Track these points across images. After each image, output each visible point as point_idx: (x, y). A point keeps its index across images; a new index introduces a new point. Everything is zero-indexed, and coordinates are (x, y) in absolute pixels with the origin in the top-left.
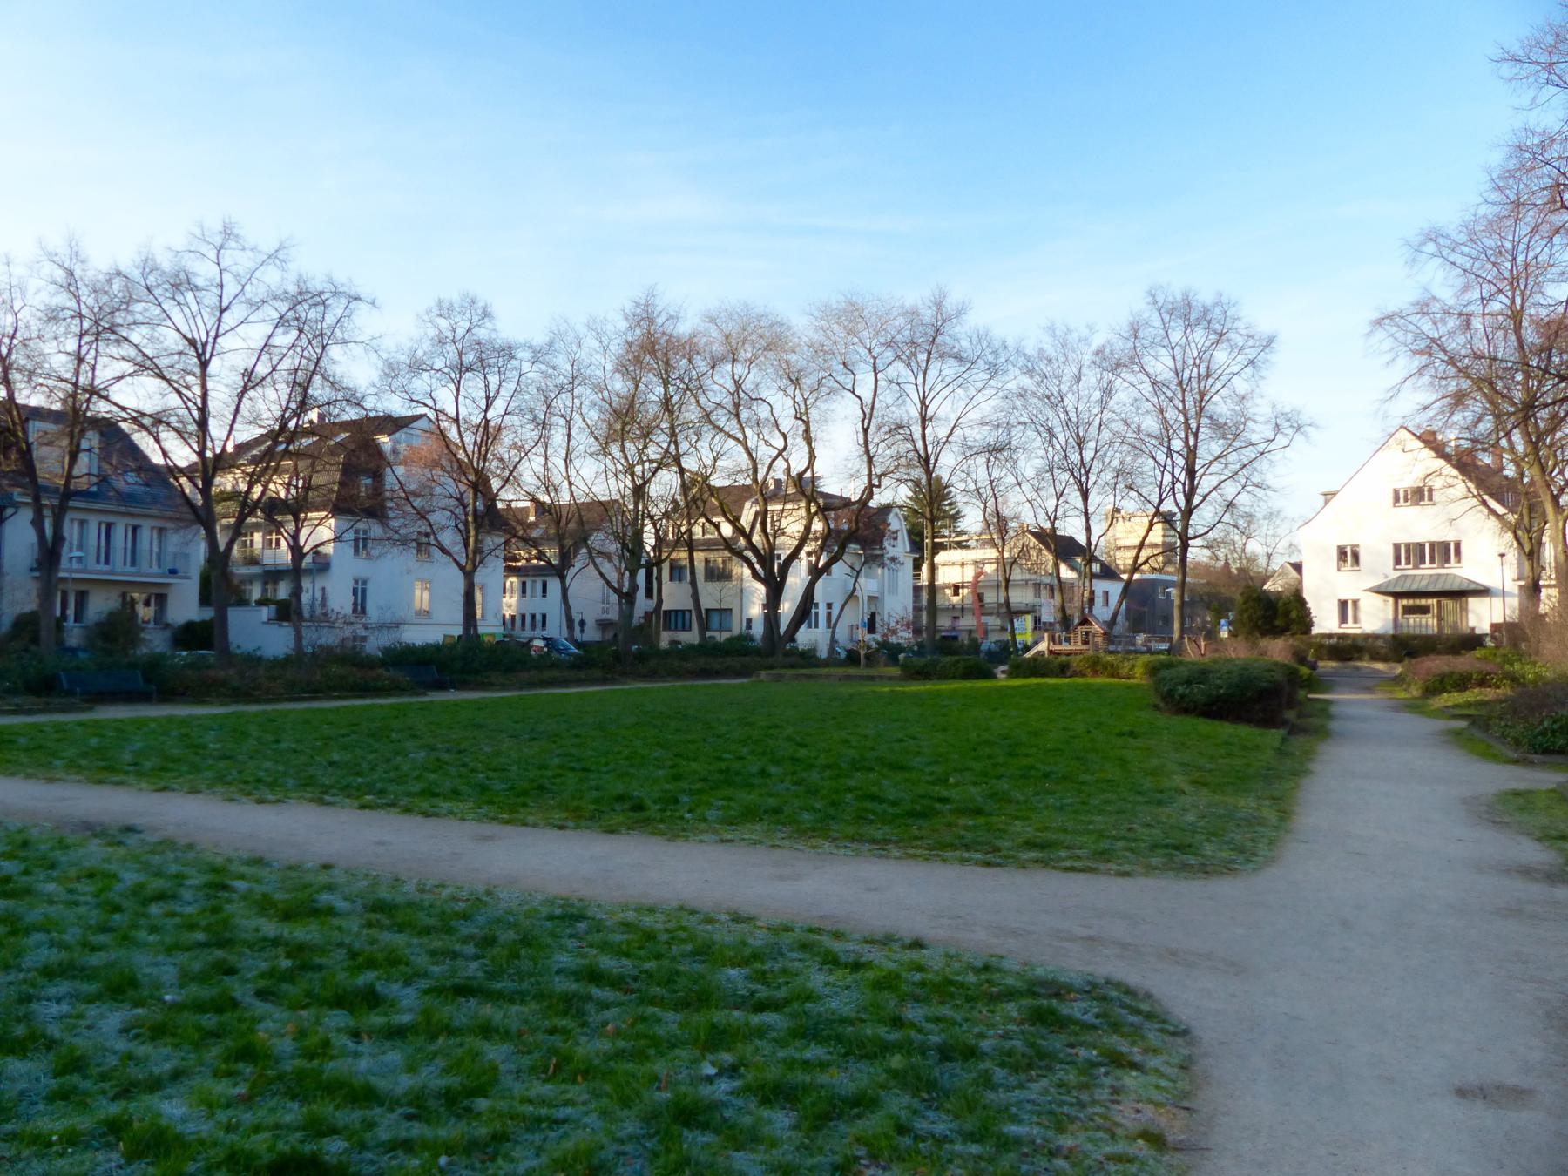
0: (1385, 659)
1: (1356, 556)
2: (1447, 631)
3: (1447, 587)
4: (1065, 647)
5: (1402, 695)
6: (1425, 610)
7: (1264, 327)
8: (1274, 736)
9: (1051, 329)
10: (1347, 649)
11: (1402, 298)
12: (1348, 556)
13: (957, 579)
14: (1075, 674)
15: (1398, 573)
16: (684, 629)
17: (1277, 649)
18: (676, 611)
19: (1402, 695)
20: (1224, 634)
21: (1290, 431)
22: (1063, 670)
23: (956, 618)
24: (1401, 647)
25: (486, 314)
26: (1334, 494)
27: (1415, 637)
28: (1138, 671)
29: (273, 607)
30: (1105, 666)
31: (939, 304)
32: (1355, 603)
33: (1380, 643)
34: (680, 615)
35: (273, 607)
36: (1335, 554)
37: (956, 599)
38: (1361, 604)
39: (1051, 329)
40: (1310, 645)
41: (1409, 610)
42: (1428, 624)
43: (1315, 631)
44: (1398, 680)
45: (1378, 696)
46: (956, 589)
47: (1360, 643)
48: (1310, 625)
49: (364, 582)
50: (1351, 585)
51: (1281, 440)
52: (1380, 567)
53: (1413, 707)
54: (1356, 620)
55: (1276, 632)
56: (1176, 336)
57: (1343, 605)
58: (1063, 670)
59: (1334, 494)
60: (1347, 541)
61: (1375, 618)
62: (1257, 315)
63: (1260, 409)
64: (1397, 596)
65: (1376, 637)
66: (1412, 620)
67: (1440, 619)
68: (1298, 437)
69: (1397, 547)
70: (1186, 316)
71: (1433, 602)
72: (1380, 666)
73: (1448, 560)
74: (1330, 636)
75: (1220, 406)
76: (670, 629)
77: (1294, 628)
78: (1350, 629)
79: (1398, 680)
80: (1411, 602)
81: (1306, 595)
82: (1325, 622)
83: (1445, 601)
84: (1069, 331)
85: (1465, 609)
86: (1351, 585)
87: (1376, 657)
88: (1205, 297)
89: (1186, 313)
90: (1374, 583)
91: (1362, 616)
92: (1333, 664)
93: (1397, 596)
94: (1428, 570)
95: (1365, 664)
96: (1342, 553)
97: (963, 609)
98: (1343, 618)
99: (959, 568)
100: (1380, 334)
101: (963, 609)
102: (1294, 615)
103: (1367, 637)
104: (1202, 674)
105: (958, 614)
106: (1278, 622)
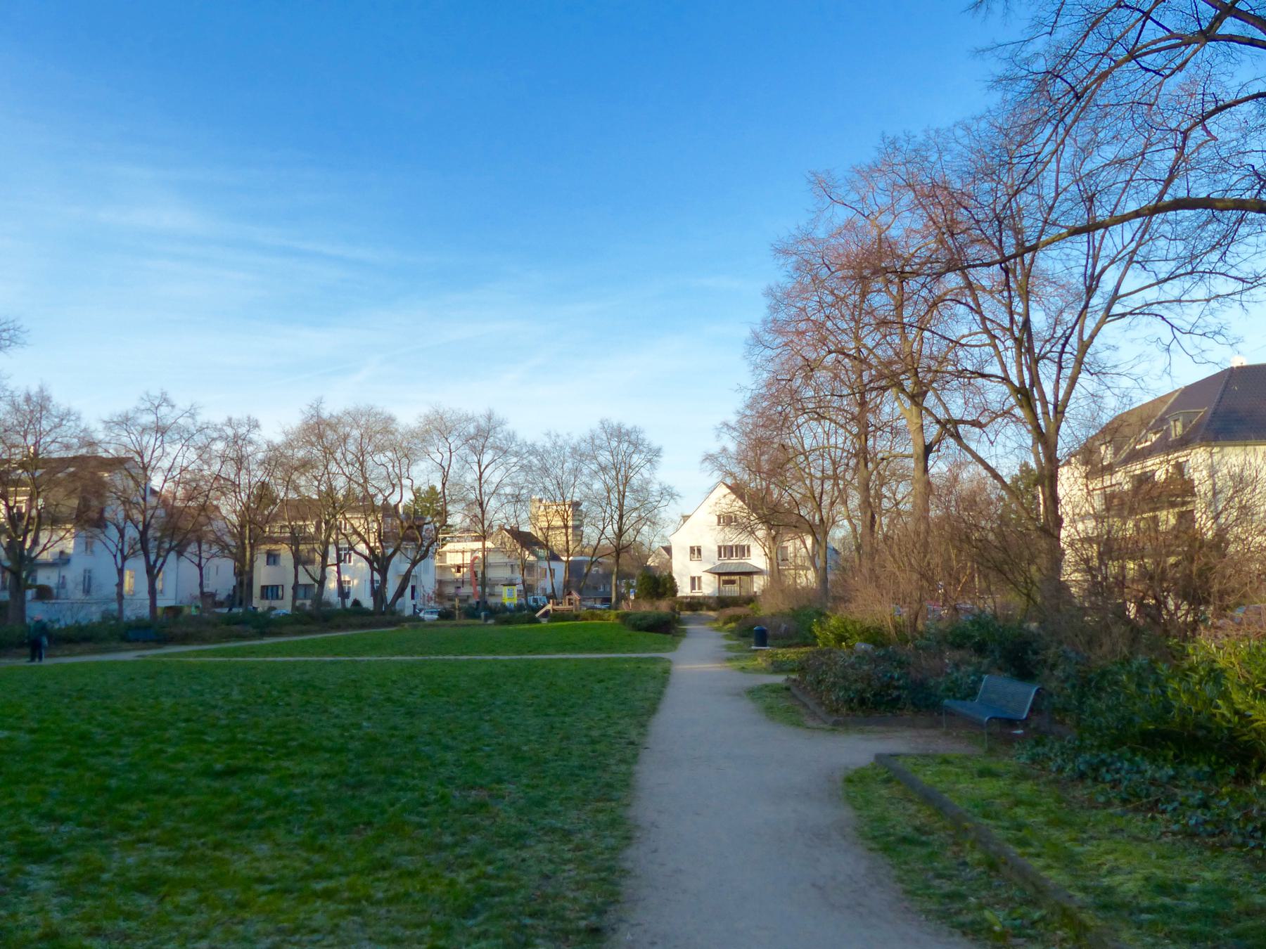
0: (714, 610)
1: (699, 551)
2: (743, 594)
3: (743, 570)
4: (560, 607)
5: (716, 625)
6: (733, 582)
7: (655, 445)
8: (669, 637)
9: (548, 434)
10: (695, 605)
11: (715, 448)
12: (696, 552)
13: (459, 562)
14: (583, 619)
15: (720, 562)
16: (277, 597)
17: (663, 606)
18: (272, 586)
19: (716, 626)
20: (632, 597)
21: (668, 497)
22: (576, 618)
23: (459, 588)
24: (721, 602)
25: (257, 426)
26: (689, 517)
27: (728, 597)
28: (612, 617)
29: (34, 590)
30: (597, 615)
31: (489, 419)
32: (699, 578)
33: (711, 601)
34: (275, 589)
35: (34, 590)
36: (689, 550)
37: (458, 575)
38: (703, 579)
39: (548, 434)
40: (677, 602)
41: (726, 582)
42: (733, 590)
43: (679, 594)
44: (716, 620)
45: (706, 627)
46: (459, 568)
47: (701, 601)
48: (675, 592)
49: (90, 571)
50: (697, 569)
51: (664, 503)
52: (711, 559)
53: (717, 630)
54: (699, 588)
55: (660, 596)
56: (614, 444)
57: (693, 579)
58: (576, 618)
59: (689, 517)
60: (694, 544)
61: (709, 587)
62: (652, 438)
63: (655, 488)
64: (720, 574)
65: (709, 597)
66: (728, 587)
67: (741, 587)
68: (672, 501)
69: (720, 548)
70: (618, 437)
71: (737, 578)
72: (712, 613)
73: (744, 555)
74: (687, 597)
75: (636, 480)
76: (267, 598)
77: (668, 593)
78: (697, 593)
79: (716, 620)
80: (726, 578)
81: (674, 575)
82: (684, 590)
83: (742, 577)
84: (558, 436)
85: (752, 581)
86: (697, 569)
87: (710, 608)
88: (628, 425)
89: (619, 434)
90: (709, 567)
91: (703, 586)
92: (688, 613)
93: (720, 574)
94: (735, 560)
95: (704, 612)
96: (692, 549)
97: (463, 582)
98: (693, 588)
99: (460, 554)
100: (707, 464)
101: (463, 582)
102: (668, 585)
103: (705, 597)
104: (644, 617)
105: (460, 585)
106: (660, 590)
